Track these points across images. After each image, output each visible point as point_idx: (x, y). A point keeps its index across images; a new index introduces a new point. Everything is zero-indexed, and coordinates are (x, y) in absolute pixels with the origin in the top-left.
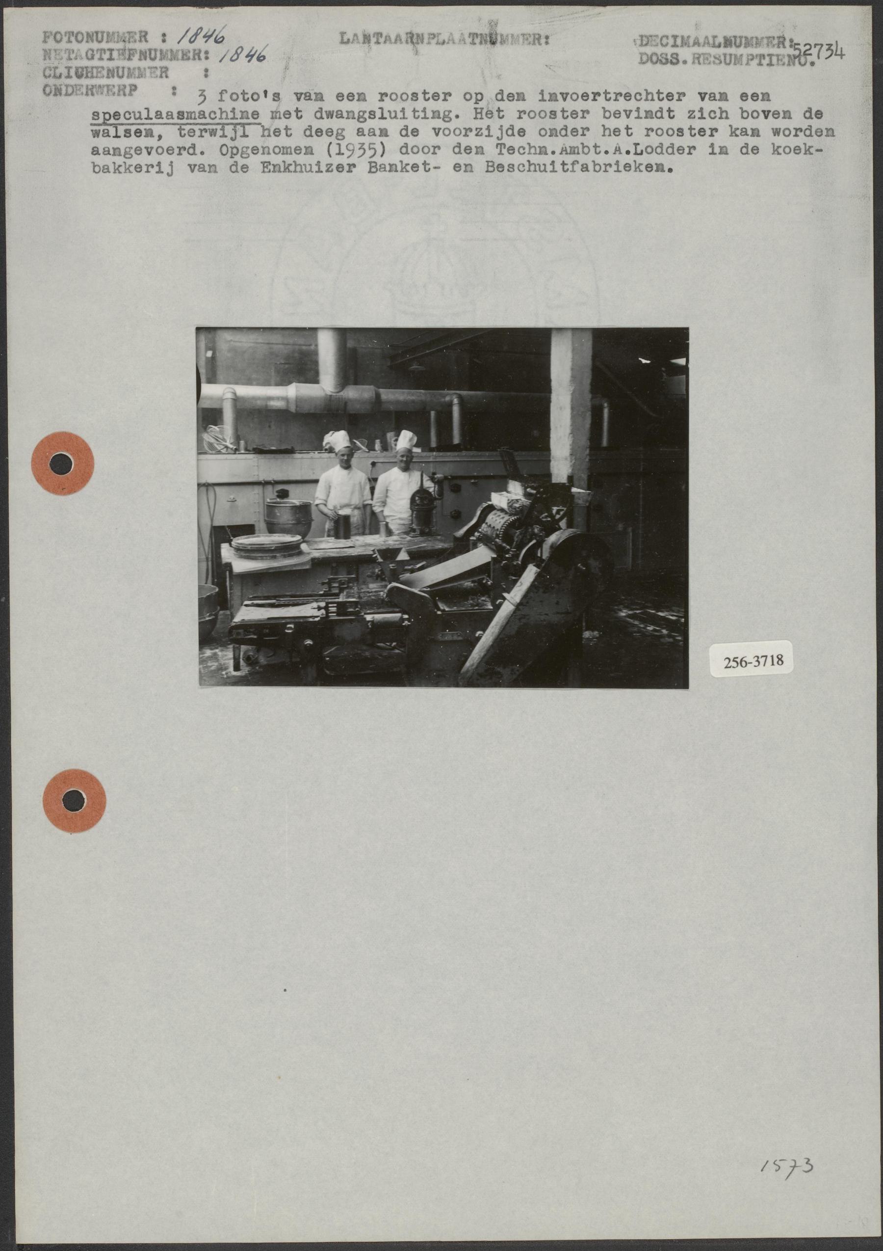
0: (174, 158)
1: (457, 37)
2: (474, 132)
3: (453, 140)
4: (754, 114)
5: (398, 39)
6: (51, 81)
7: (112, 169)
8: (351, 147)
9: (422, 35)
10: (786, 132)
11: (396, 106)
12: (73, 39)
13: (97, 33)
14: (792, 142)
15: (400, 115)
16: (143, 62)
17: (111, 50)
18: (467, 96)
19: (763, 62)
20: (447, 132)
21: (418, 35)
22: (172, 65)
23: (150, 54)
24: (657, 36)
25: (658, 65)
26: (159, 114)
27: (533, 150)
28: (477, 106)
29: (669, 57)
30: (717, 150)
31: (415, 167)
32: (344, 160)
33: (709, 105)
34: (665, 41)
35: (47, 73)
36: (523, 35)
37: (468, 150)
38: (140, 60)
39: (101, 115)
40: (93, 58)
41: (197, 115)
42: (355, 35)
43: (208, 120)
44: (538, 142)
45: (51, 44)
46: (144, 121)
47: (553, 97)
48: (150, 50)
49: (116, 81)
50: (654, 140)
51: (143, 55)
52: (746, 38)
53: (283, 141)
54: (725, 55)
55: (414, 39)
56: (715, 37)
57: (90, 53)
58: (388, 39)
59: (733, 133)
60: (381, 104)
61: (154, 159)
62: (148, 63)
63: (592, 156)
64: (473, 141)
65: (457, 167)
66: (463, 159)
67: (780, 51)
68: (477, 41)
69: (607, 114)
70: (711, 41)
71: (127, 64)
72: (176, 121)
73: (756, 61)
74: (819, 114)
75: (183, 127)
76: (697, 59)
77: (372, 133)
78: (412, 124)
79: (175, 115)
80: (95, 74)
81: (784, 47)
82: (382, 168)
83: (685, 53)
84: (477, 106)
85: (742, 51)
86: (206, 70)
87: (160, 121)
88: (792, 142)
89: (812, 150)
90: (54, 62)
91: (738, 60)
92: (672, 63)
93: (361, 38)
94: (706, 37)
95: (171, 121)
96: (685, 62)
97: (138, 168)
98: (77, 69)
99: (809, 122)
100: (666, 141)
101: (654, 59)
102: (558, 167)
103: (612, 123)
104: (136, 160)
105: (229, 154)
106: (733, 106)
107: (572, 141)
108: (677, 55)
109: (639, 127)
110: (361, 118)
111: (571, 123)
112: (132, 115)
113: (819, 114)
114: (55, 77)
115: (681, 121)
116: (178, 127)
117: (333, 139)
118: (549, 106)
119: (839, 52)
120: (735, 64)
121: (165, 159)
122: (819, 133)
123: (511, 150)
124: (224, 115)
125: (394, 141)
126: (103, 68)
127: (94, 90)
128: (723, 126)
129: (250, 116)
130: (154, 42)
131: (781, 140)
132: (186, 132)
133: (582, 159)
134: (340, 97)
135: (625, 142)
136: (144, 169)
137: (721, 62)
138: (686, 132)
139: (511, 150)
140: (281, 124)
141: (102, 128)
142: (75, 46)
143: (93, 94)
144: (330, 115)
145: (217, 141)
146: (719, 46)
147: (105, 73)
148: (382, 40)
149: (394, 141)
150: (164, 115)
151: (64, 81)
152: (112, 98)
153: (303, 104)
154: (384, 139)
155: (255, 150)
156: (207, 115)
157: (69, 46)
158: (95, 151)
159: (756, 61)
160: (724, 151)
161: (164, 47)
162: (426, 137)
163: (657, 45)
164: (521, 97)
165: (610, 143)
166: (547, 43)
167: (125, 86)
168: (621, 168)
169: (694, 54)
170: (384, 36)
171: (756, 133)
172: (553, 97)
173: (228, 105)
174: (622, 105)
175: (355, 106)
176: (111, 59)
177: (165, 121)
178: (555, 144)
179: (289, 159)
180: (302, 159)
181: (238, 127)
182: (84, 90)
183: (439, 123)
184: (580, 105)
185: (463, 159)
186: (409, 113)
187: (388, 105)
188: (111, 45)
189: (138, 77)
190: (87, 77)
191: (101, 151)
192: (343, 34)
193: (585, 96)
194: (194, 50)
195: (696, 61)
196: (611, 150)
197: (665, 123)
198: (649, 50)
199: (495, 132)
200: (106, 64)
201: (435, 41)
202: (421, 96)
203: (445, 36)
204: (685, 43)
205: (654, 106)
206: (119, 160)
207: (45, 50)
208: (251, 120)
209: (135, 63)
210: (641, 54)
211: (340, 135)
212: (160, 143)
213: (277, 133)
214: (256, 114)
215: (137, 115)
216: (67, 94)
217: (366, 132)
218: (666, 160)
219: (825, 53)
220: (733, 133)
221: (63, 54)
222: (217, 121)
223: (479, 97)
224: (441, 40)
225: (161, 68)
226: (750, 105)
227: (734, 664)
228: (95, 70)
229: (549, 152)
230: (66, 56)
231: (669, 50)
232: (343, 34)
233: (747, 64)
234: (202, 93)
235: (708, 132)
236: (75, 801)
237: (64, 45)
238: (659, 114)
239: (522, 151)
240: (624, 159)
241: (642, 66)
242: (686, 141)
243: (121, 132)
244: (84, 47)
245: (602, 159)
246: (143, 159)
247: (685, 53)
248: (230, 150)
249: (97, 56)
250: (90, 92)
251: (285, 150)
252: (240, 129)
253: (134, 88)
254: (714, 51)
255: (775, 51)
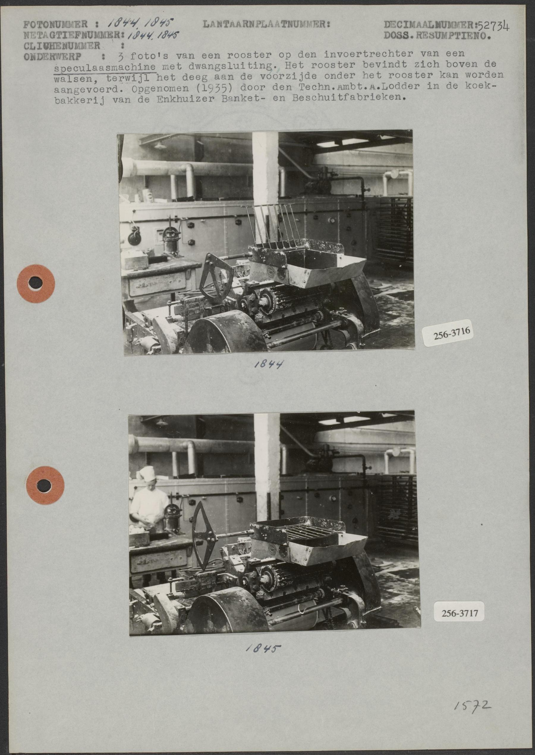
0: (105, 94)
1: (274, 23)
2: (286, 76)
3: (273, 82)
4: (455, 65)
5: (238, 24)
6: (29, 52)
7: (67, 101)
8: (211, 87)
9: (253, 21)
10: (474, 75)
11: (239, 61)
12: (42, 26)
13: (56, 22)
14: (478, 81)
15: (240, 66)
16: (85, 39)
17: (65, 32)
18: (281, 55)
19: (459, 37)
20: (269, 77)
21: (250, 22)
22: (103, 42)
23: (89, 34)
24: (395, 21)
25: (396, 39)
26: (95, 68)
27: (321, 87)
28: (287, 61)
29: (403, 35)
30: (432, 86)
31: (250, 98)
32: (207, 94)
33: (427, 59)
34: (400, 25)
35: (27, 47)
36: (314, 21)
37: (282, 87)
38: (83, 38)
39: (60, 69)
40: (54, 37)
41: (118, 68)
42: (213, 22)
43: (125, 71)
44: (324, 82)
45: (29, 29)
46: (85, 72)
47: (333, 55)
48: (89, 32)
49: (67, 51)
50: (394, 81)
51: (85, 35)
52: (449, 22)
53: (169, 83)
54: (436, 32)
55: (249, 24)
56: (430, 22)
57: (52, 34)
58: (232, 24)
59: (442, 76)
60: (229, 60)
61: (92, 95)
62: (88, 40)
63: (357, 90)
64: (284, 82)
65: (275, 98)
66: (279, 93)
67: (470, 30)
68: (287, 25)
69: (366, 65)
70: (428, 25)
71: (74, 40)
72: (105, 72)
73: (455, 36)
74: (494, 64)
75: (109, 75)
76: (419, 35)
77: (223, 77)
78: (247, 71)
79: (105, 68)
80: (55, 47)
81: (472, 28)
82: (230, 99)
83: (412, 32)
84: (287, 61)
85: (447, 30)
86: (123, 44)
87: (96, 72)
88: (478, 81)
89: (490, 86)
90: (29, 40)
91: (444, 36)
92: (404, 38)
93: (216, 24)
94: (425, 22)
95: (102, 72)
96: (412, 37)
97: (83, 100)
98: (45, 43)
99: (488, 69)
100: (402, 80)
101: (394, 35)
102: (337, 97)
103: (369, 70)
104: (80, 96)
105: (138, 91)
106: (442, 59)
107: (344, 82)
108: (407, 33)
109: (385, 73)
110: (216, 68)
111: (344, 70)
112: (79, 68)
113: (494, 64)
114: (31, 49)
115: (411, 68)
116: (106, 75)
117: (200, 82)
118: (330, 60)
119: (506, 27)
120: (442, 38)
121: (99, 95)
122: (494, 76)
123: (308, 87)
124: (134, 68)
125: (237, 83)
126: (60, 43)
127: (55, 57)
128: (436, 71)
129: (150, 68)
130: (91, 27)
131: (471, 80)
132: (111, 78)
133: (351, 92)
134: (204, 56)
135: (377, 82)
136: (86, 101)
137: (434, 37)
138: (414, 75)
139: (308, 87)
140: (169, 73)
141: (60, 76)
142: (43, 30)
143: (54, 59)
144: (198, 66)
145: (131, 84)
146: (433, 27)
147: (62, 46)
148: (228, 25)
149: (237, 83)
150: (98, 68)
151: (36, 51)
152: (66, 61)
153: (182, 61)
154: (231, 82)
155: (153, 89)
156: (124, 68)
157: (40, 30)
158: (57, 90)
159: (455, 36)
160: (436, 86)
161: (97, 30)
162: (256, 81)
163: (395, 27)
164: (313, 55)
165: (367, 82)
166: (329, 26)
167: (73, 54)
168: (375, 98)
169: (418, 32)
170: (230, 22)
171: (455, 75)
172: (333, 55)
173: (136, 62)
174: (374, 59)
175: (214, 62)
176: (65, 37)
177: (99, 72)
178: (334, 83)
179: (174, 94)
180: (181, 94)
181: (143, 75)
182: (49, 57)
183: (264, 71)
184: (349, 60)
185: (279, 93)
186: (246, 66)
187: (234, 61)
188: (65, 29)
189: (82, 49)
190: (51, 49)
191: (60, 90)
192: (205, 21)
193: (352, 55)
194: (115, 32)
195: (419, 37)
196: (369, 87)
197: (401, 70)
198: (390, 30)
199: (298, 77)
200: (62, 41)
201: (261, 25)
202: (253, 55)
203: (267, 23)
204: (412, 25)
205: (394, 60)
206: (71, 96)
207: (25, 33)
208: (151, 71)
209: (80, 40)
210: (386, 32)
211: (204, 79)
212: (96, 86)
213: (166, 78)
214: (153, 67)
215: (82, 69)
216: (38, 59)
217: (220, 77)
218: (403, 93)
219: (497, 27)
220: (442, 76)
221: (36, 35)
222: (130, 71)
223: (288, 55)
224: (264, 25)
225: (95, 43)
226: (452, 59)
227: (448, 614)
228: (55, 45)
229: (331, 88)
230: (38, 36)
231: (403, 30)
232: (205, 21)
233: (450, 38)
234: (121, 55)
235: (427, 75)
236: (45, 485)
237: (36, 29)
238: (397, 65)
239: (314, 88)
240: (376, 92)
241: (386, 39)
242: (413, 81)
243: (72, 79)
244: (49, 30)
245: (363, 92)
246: (86, 95)
247: (412, 32)
248: (138, 89)
249: (57, 36)
250: (52, 58)
251: (170, 89)
252: (143, 76)
253: (79, 55)
254: (430, 30)
255: (467, 30)
